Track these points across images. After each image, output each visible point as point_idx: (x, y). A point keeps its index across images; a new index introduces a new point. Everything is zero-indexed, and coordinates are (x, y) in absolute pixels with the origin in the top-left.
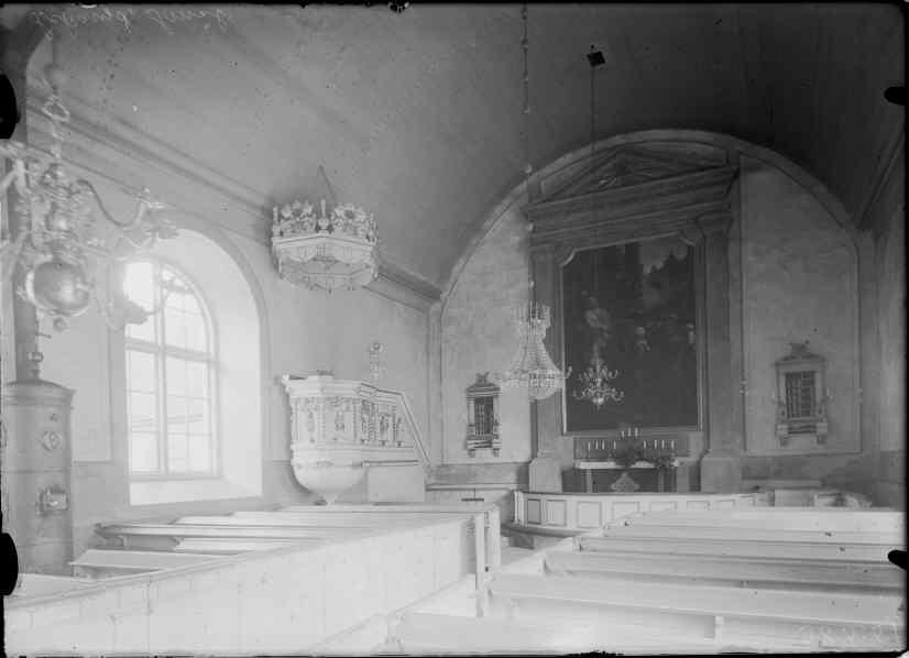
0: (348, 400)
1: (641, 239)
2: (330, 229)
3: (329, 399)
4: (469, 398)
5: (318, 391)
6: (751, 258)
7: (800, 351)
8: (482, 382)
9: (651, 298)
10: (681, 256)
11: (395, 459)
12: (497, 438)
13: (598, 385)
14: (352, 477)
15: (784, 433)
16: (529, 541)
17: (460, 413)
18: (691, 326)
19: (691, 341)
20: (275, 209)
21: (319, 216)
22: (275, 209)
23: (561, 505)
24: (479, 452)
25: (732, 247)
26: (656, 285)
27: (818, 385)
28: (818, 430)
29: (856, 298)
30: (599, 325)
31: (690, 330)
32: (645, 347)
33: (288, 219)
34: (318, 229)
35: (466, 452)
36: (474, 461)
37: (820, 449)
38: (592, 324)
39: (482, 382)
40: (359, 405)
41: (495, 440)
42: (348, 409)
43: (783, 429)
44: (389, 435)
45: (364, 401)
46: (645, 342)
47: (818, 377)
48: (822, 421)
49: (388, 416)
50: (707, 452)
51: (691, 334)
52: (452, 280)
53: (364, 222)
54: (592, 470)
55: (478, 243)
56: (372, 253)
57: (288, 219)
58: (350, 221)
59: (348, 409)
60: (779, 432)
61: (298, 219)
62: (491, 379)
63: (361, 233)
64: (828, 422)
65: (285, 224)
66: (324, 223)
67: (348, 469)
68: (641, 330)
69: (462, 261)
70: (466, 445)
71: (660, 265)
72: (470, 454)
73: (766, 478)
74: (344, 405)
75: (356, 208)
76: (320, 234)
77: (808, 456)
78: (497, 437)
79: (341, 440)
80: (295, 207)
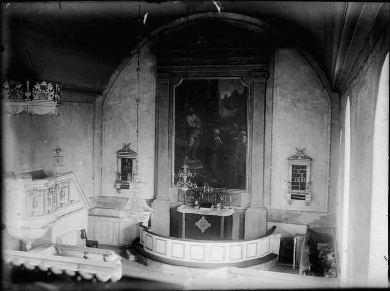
0: (40, 191)
1: (220, 78)
2: (32, 98)
3: (29, 191)
4: (118, 157)
6: (278, 98)
7: (301, 154)
8: (126, 149)
9: (225, 113)
10: (241, 92)
13: (185, 180)
15: (119, 187)
16: (145, 260)
17: (113, 166)
18: (245, 133)
19: (244, 141)
21: (25, 91)
23: (164, 242)
25: (269, 91)
26: (228, 108)
27: (308, 174)
28: (306, 199)
29: (329, 129)
30: (194, 125)
31: (244, 135)
32: (219, 141)
34: (24, 97)
35: (115, 189)
36: (120, 195)
37: (308, 209)
38: (190, 124)
39: (126, 149)
46: (219, 138)
47: (308, 170)
48: (308, 194)
49: (65, 187)
50: (249, 207)
51: (245, 137)
52: (110, 84)
54: (186, 213)
55: (126, 63)
57: (7, 89)
58: (44, 91)
59: (40, 195)
61: (12, 90)
62: (131, 147)
64: (311, 195)
66: (28, 94)
68: (217, 131)
69: (117, 72)
70: (115, 186)
71: (229, 95)
73: (280, 222)
77: (301, 212)
79: (35, 214)
80: (12, 83)
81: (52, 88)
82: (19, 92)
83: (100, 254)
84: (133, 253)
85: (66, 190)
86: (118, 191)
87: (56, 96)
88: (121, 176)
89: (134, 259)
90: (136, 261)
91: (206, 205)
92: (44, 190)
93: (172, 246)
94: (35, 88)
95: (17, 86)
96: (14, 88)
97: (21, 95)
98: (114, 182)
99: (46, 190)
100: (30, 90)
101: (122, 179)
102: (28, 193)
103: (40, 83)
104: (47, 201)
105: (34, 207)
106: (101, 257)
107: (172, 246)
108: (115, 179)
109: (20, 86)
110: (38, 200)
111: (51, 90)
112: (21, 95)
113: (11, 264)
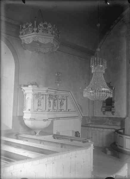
0: (43, 95)
5: (45, 92)
11: (72, 116)
12: (114, 108)
14: (44, 124)
15: (104, 110)
20: (21, 26)
22: (21, 26)
24: (106, 113)
33: (25, 29)
34: (33, 31)
35: (102, 112)
36: (105, 116)
40: (48, 97)
41: (112, 109)
42: (43, 98)
43: (104, 109)
44: (64, 107)
45: (50, 95)
49: (64, 100)
53: (51, 28)
56: (54, 39)
57: (25, 29)
60: (103, 110)
63: (49, 32)
65: (23, 30)
66: (35, 29)
67: (43, 122)
70: (102, 109)
72: (103, 113)
74: (42, 97)
75: (48, 23)
76: (34, 33)
78: (113, 107)
81: (51, 26)
82: (30, 29)
83: (81, 141)
84: (109, 150)
85: (65, 102)
86: (104, 113)
87: (53, 32)
88: (105, 104)
89: (110, 154)
90: (112, 155)
91: (101, 60)
92: (45, 95)
93: (119, 138)
94: (39, 25)
95: (30, 25)
96: (28, 27)
97: (31, 30)
98: (101, 107)
99: (47, 95)
100: (36, 27)
101: (106, 105)
102: (35, 96)
103: (43, 22)
104: (48, 103)
105: (38, 105)
106: (30, 108)
107: (119, 138)
108: (102, 105)
109: (31, 25)
110: (41, 101)
111: (50, 27)
112: (31, 30)
113: (93, 173)
